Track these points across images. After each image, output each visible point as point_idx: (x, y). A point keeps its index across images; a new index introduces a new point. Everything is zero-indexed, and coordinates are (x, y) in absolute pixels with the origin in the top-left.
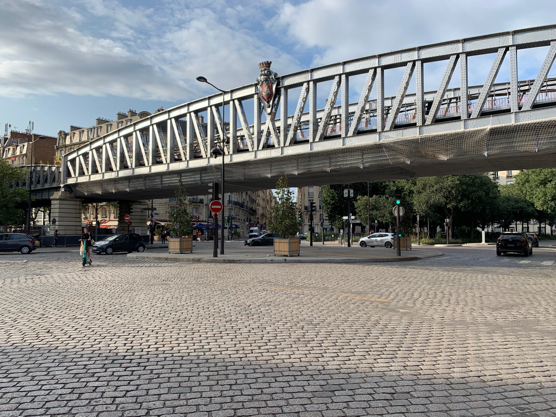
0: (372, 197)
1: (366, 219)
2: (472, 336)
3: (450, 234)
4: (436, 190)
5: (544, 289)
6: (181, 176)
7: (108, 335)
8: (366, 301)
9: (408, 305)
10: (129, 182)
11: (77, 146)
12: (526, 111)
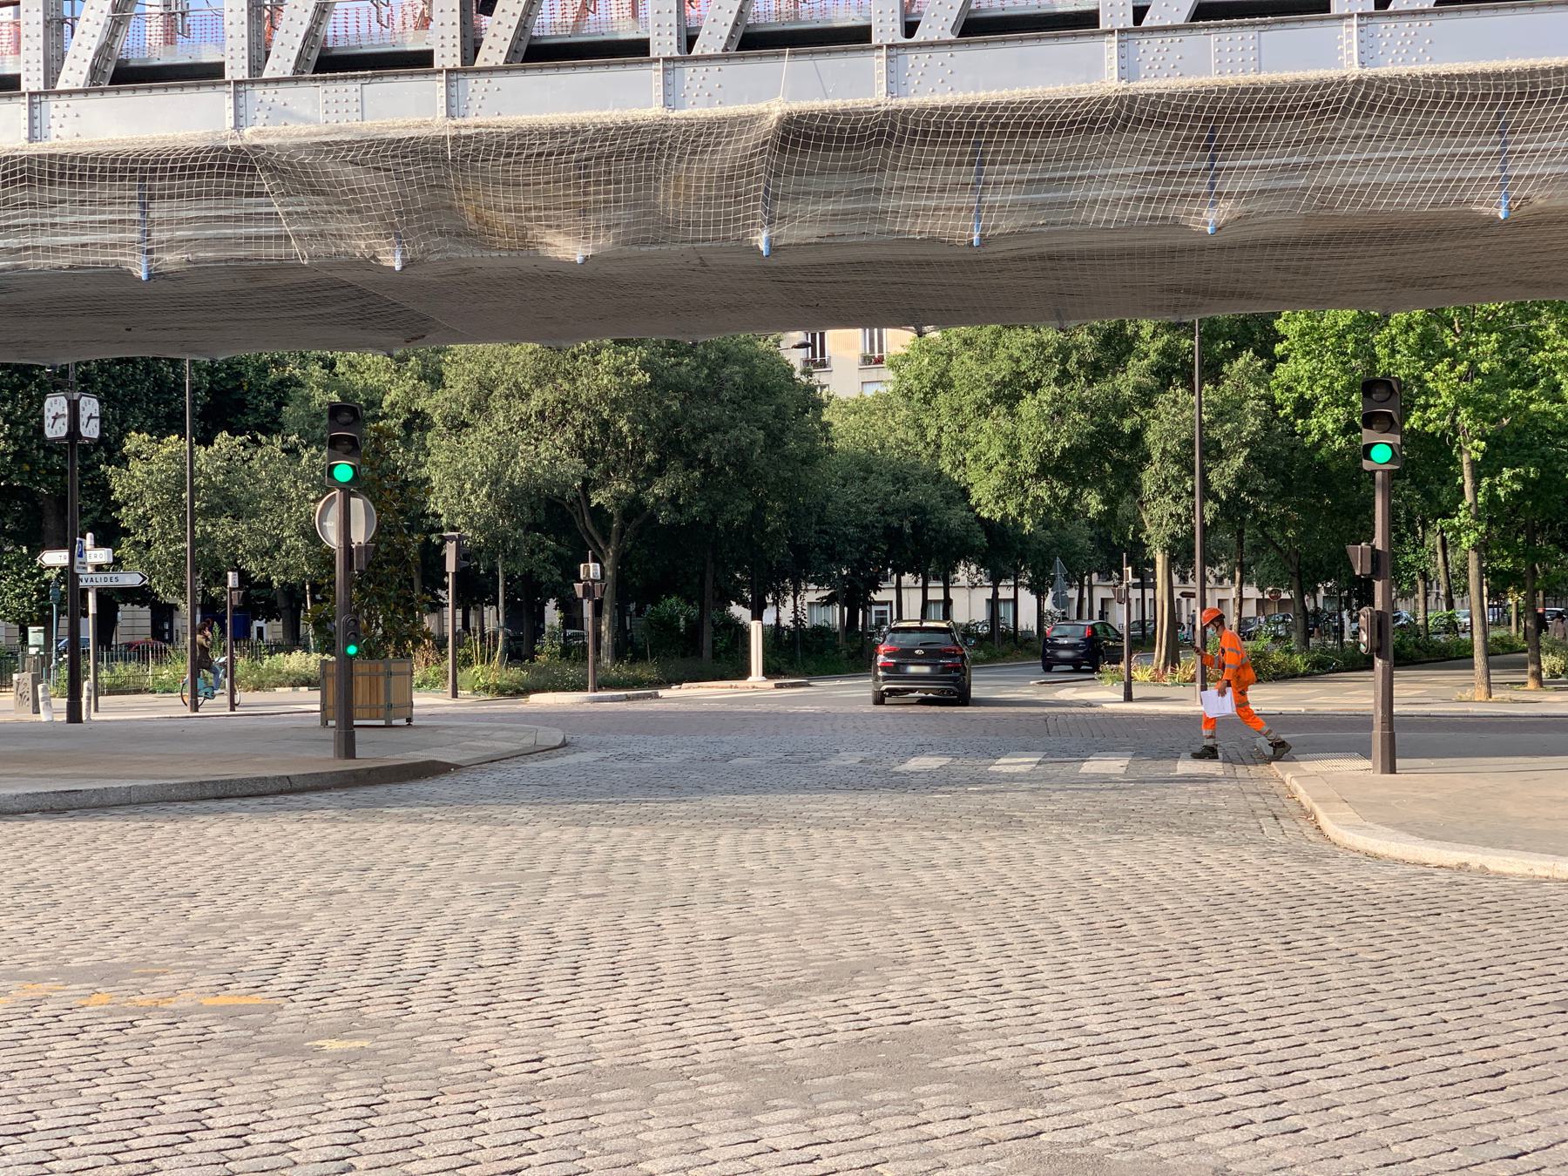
0: (207, 441)
1: (177, 559)
2: (666, 1135)
3: (606, 638)
4: (541, 414)
5: (989, 882)
8: (146, 1013)
9: (372, 1013)
12: (932, 45)
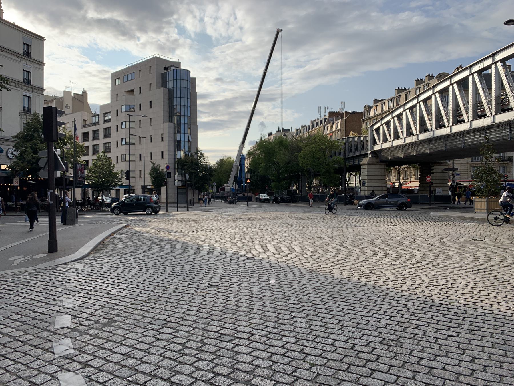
6: (486, 133)
7: (423, 282)
10: (430, 144)
11: (380, 116)
